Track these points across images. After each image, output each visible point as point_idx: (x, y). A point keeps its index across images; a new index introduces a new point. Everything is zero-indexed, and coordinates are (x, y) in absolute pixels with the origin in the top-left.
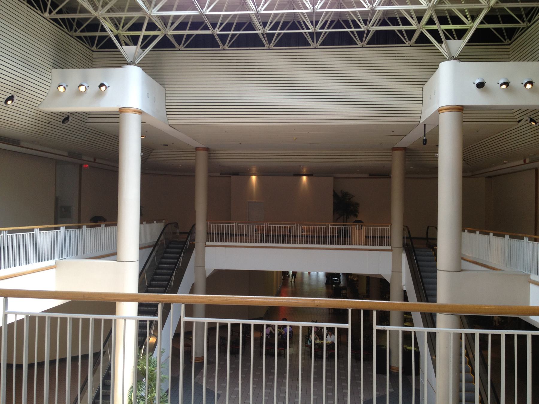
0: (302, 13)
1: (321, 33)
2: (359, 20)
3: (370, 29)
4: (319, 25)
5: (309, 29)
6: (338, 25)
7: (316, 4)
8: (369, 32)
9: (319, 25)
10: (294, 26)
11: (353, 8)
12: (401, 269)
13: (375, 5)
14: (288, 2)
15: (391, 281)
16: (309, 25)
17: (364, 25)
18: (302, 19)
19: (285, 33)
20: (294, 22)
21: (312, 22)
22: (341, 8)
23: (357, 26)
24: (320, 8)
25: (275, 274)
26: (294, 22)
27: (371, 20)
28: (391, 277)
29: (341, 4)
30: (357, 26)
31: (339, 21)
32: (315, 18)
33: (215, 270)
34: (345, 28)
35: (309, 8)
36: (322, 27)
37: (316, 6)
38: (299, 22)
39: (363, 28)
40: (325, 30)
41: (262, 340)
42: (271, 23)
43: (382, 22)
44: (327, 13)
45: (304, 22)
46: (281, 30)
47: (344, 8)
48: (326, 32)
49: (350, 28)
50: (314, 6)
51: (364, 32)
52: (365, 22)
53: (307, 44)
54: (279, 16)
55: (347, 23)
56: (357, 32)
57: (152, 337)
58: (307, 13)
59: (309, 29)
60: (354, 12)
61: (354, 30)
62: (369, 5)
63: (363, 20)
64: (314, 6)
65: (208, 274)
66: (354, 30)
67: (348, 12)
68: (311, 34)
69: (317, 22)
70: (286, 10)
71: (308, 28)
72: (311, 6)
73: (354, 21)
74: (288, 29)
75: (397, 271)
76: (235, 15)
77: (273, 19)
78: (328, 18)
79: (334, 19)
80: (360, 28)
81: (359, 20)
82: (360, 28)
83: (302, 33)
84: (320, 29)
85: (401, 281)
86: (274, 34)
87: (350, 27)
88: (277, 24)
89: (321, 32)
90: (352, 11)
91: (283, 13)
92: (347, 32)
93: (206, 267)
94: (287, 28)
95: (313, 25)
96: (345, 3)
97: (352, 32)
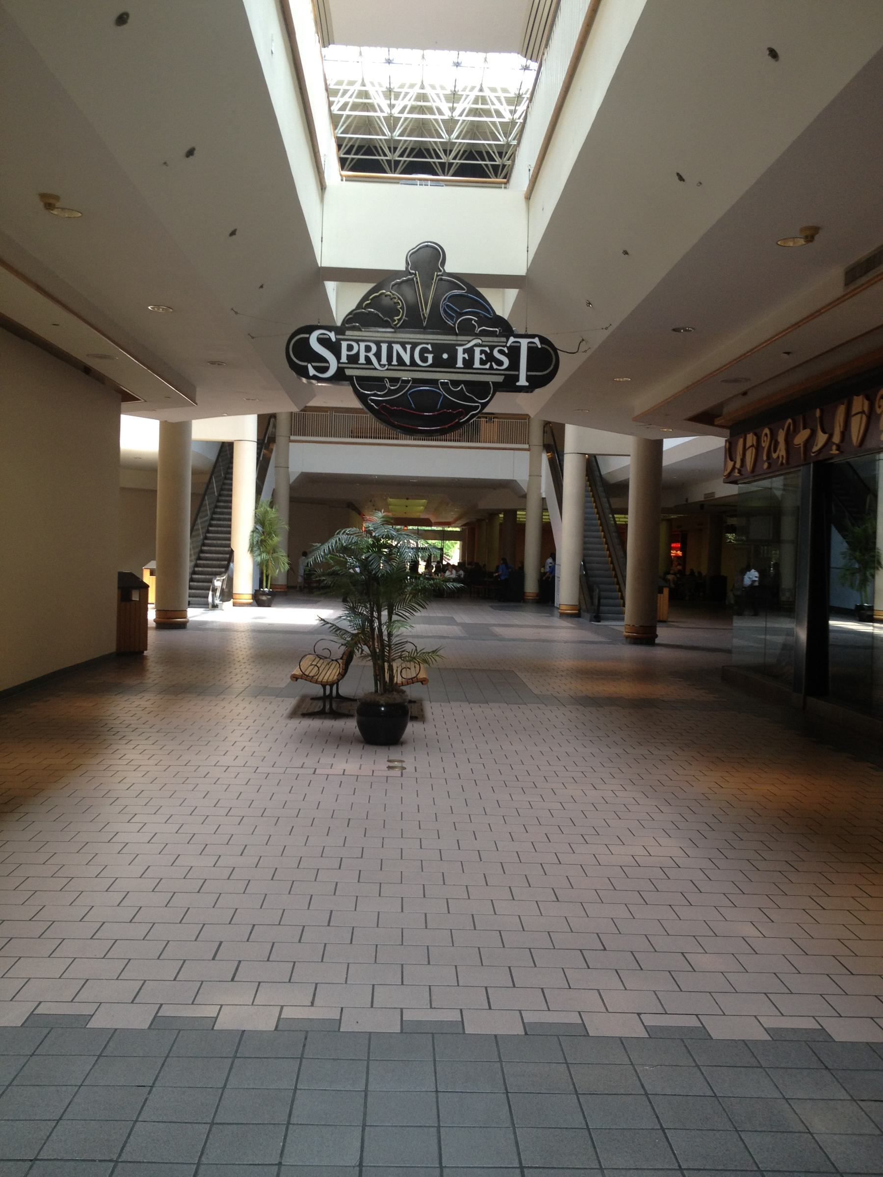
0: (381, 140)
1: (400, 161)
2: (494, 152)
3: (505, 164)
4: (398, 152)
5: (387, 156)
6: (420, 154)
7: (394, 131)
8: (504, 166)
9: (398, 152)
10: (369, 152)
11: (489, 140)
12: (540, 473)
13: (510, 139)
14: (418, 127)
15: (528, 489)
16: (387, 151)
17: (500, 159)
18: (379, 144)
19: (359, 159)
20: (420, 149)
21: (389, 148)
22: (422, 137)
23: (492, 159)
24: (398, 136)
25: (230, 493)
26: (369, 146)
27: (506, 153)
28: (528, 485)
29: (475, 133)
30: (492, 159)
31: (471, 151)
32: (393, 146)
33: (302, 473)
34: (478, 160)
35: (444, 137)
36: (401, 155)
37: (394, 134)
38: (375, 147)
39: (498, 161)
40: (457, 161)
41: (550, 560)
42: (346, 145)
43: (418, 151)
44: (406, 141)
45: (381, 147)
46: (354, 154)
47: (479, 140)
48: (405, 161)
49: (433, 158)
50: (392, 133)
51: (499, 166)
52: (500, 154)
53: (486, 176)
54: (353, 140)
55: (480, 153)
56: (491, 165)
57: (132, 597)
58: (385, 139)
59: (387, 156)
60: (490, 145)
61: (488, 163)
62: (504, 138)
63: (498, 153)
64: (392, 133)
65: (292, 479)
66: (488, 163)
67: (483, 144)
68: (389, 162)
69: (395, 149)
70: (360, 134)
71: (385, 155)
72: (447, 136)
73: (488, 153)
74: (362, 155)
75: (535, 475)
76: (357, 139)
77: (348, 142)
78: (461, 148)
79: (414, 147)
80: (495, 161)
81: (494, 152)
82: (495, 161)
83: (378, 160)
84: (399, 157)
85: (540, 488)
86: (348, 158)
87: (484, 160)
88: (352, 147)
89: (400, 161)
90: (433, 141)
91: (411, 141)
92: (480, 164)
93: (290, 470)
94: (361, 153)
95: (390, 152)
96: (480, 133)
97: (486, 165)
